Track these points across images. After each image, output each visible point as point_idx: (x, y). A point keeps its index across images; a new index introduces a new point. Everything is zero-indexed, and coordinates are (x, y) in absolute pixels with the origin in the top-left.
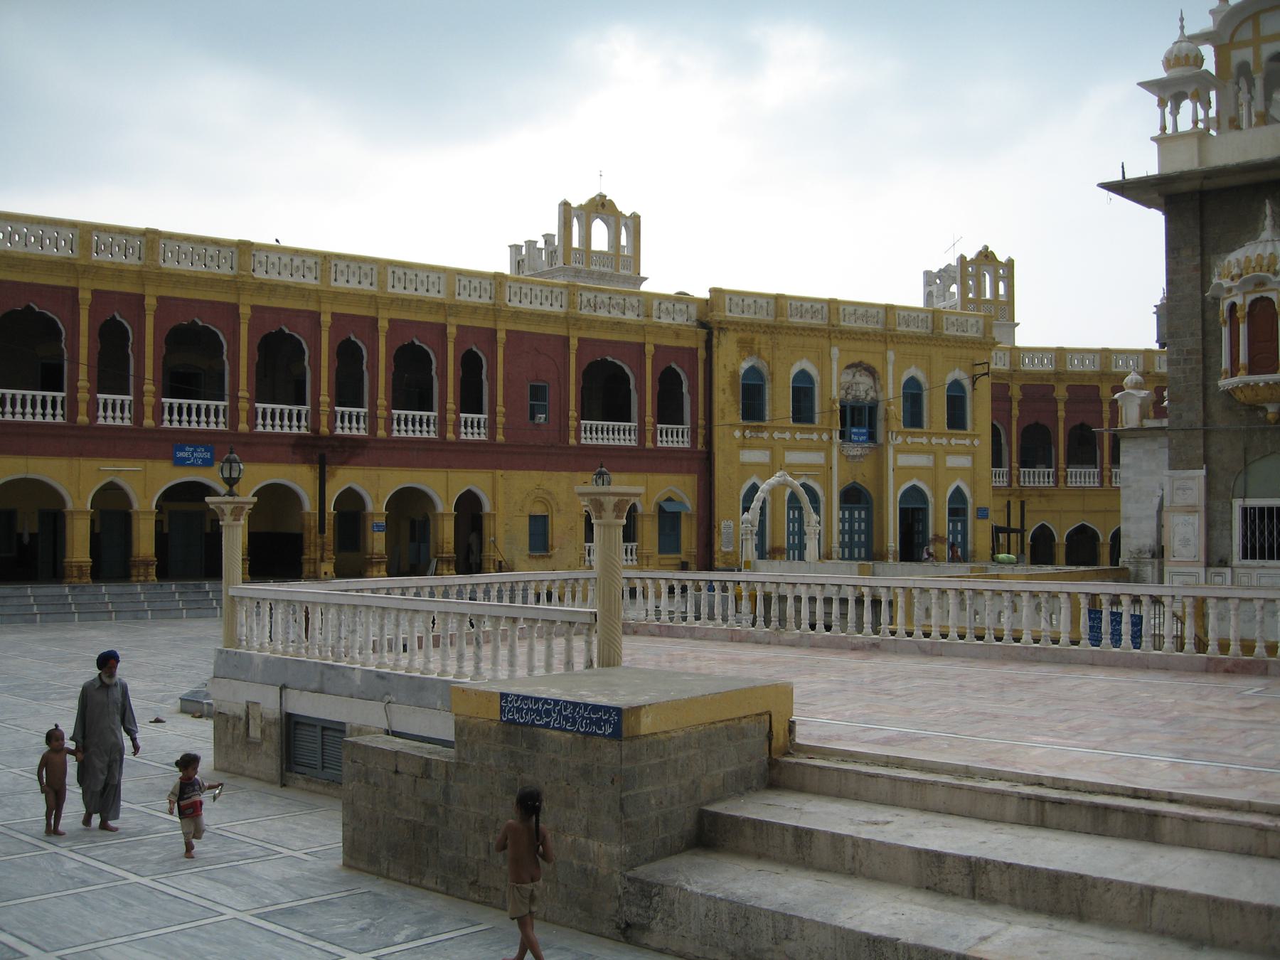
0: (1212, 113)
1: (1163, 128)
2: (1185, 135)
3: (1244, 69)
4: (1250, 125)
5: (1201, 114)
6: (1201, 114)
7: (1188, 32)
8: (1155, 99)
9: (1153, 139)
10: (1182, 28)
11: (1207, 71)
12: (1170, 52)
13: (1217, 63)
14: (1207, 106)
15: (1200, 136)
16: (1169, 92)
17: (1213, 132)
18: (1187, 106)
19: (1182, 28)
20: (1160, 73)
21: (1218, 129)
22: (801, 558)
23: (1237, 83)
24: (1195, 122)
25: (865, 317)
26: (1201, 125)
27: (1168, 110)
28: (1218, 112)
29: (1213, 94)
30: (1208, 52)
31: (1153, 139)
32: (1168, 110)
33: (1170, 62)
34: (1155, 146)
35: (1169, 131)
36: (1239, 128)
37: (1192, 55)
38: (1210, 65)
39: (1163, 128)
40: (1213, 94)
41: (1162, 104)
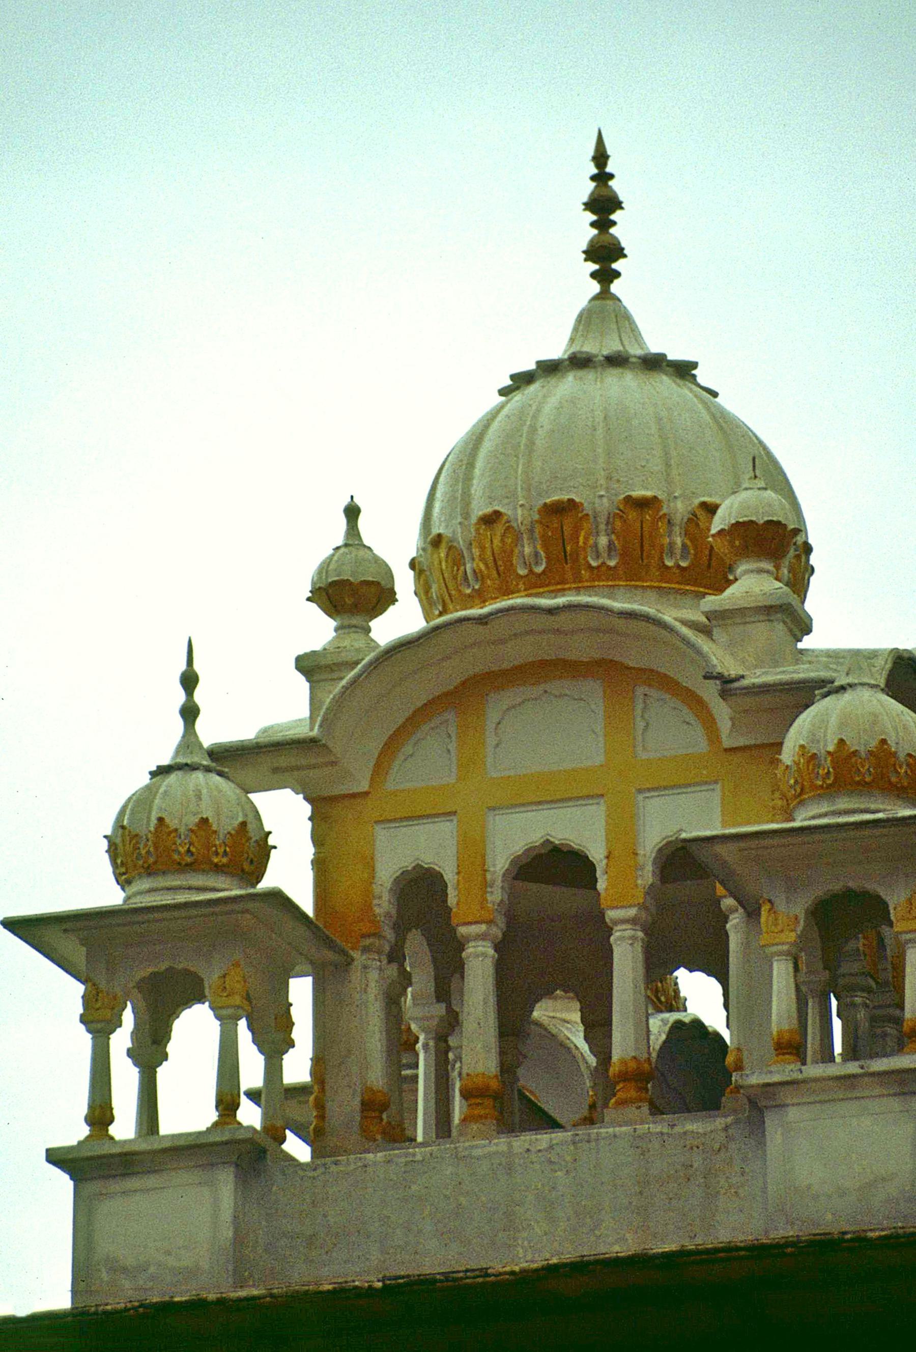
0: (297, 1067)
1: (100, 1115)
2: (191, 1151)
3: (421, 891)
4: (442, 1126)
5: (252, 1069)
6: (252, 1069)
7: (210, 733)
8: (73, 991)
9: (56, 1158)
10: (190, 713)
11: (278, 898)
12: (140, 802)
13: (320, 865)
14: (275, 1040)
15: (233, 1153)
16: (134, 956)
17: (297, 1148)
18: (195, 1030)
19: (190, 713)
20: (97, 888)
21: (315, 1138)
22: (449, 1136)
23: (396, 956)
24: (227, 1104)
25: (190, 1139)
26: (250, 1115)
27: (121, 1040)
28: (319, 1062)
29: (301, 992)
30: (285, 816)
31: (56, 1158)
32: (121, 1040)
33: (136, 847)
34: (62, 1185)
35: (124, 1127)
36: (398, 1135)
37: (225, 825)
38: (291, 872)
39: (100, 1115)
40: (301, 992)
41: (98, 1020)
